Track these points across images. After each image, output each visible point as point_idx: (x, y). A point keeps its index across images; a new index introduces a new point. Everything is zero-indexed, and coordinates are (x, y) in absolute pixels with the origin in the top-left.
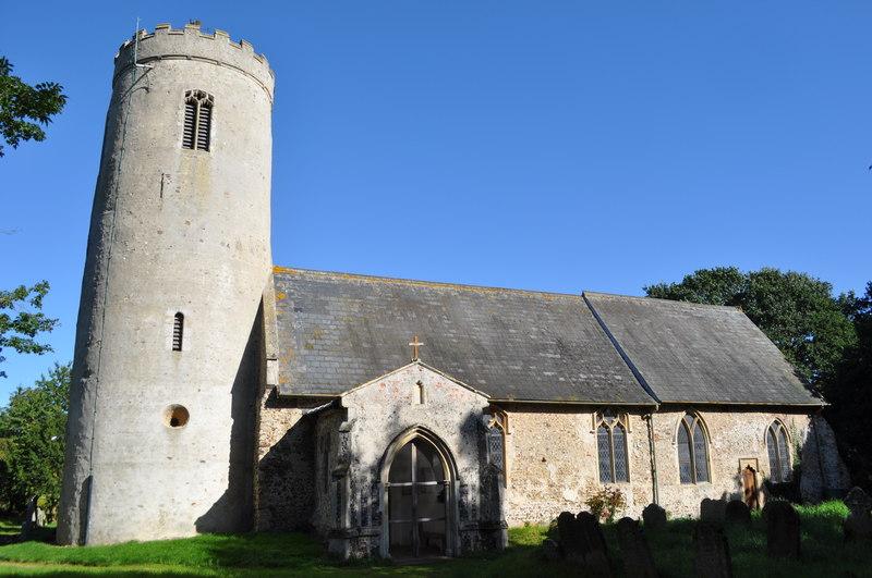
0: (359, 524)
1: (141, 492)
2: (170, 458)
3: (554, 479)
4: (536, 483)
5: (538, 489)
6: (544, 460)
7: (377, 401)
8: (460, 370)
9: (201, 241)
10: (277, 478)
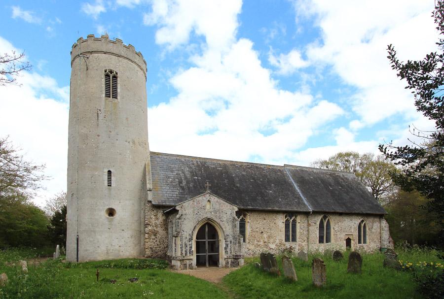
0: (184, 255)
3: (266, 240)
6: (262, 232)
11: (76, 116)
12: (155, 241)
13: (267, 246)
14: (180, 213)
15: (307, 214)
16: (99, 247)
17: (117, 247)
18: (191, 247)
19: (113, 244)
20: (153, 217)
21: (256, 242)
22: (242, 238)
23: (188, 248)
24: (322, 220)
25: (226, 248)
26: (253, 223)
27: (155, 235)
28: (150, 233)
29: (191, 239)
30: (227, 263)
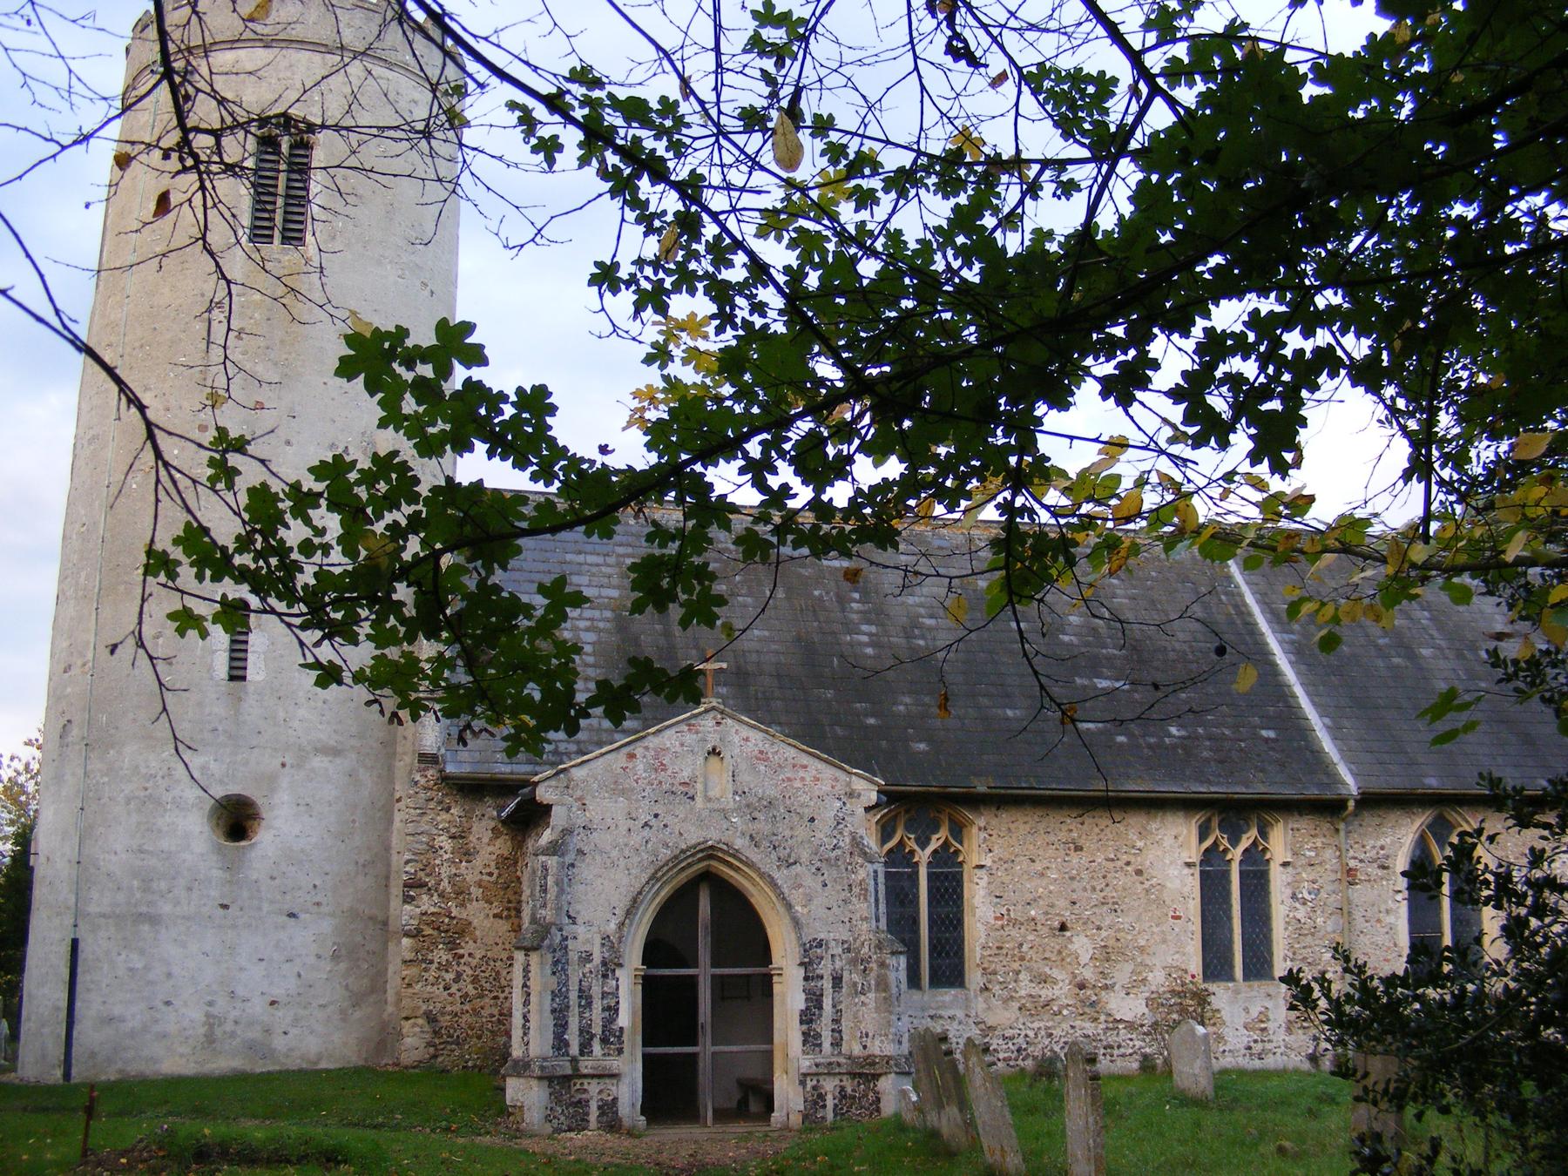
0: (574, 1049)
1: (169, 975)
2: (225, 907)
3: (1088, 974)
4: (1044, 980)
5: (1046, 993)
6: (1063, 928)
7: (617, 789)
8: (872, 721)
9: (288, 443)
10: (441, 955)
11: (113, 339)
12: (450, 976)
13: (1091, 1008)
14: (558, 817)
15: (1329, 808)
16: (168, 1003)
17: (258, 1007)
18: (613, 1010)
19: (240, 991)
20: (444, 842)
21: (1025, 987)
22: (903, 960)
23: (597, 1014)
24: (1421, 843)
25: (807, 1017)
26: (1008, 870)
27: (452, 945)
28: (428, 931)
29: (609, 968)
30: (817, 1100)
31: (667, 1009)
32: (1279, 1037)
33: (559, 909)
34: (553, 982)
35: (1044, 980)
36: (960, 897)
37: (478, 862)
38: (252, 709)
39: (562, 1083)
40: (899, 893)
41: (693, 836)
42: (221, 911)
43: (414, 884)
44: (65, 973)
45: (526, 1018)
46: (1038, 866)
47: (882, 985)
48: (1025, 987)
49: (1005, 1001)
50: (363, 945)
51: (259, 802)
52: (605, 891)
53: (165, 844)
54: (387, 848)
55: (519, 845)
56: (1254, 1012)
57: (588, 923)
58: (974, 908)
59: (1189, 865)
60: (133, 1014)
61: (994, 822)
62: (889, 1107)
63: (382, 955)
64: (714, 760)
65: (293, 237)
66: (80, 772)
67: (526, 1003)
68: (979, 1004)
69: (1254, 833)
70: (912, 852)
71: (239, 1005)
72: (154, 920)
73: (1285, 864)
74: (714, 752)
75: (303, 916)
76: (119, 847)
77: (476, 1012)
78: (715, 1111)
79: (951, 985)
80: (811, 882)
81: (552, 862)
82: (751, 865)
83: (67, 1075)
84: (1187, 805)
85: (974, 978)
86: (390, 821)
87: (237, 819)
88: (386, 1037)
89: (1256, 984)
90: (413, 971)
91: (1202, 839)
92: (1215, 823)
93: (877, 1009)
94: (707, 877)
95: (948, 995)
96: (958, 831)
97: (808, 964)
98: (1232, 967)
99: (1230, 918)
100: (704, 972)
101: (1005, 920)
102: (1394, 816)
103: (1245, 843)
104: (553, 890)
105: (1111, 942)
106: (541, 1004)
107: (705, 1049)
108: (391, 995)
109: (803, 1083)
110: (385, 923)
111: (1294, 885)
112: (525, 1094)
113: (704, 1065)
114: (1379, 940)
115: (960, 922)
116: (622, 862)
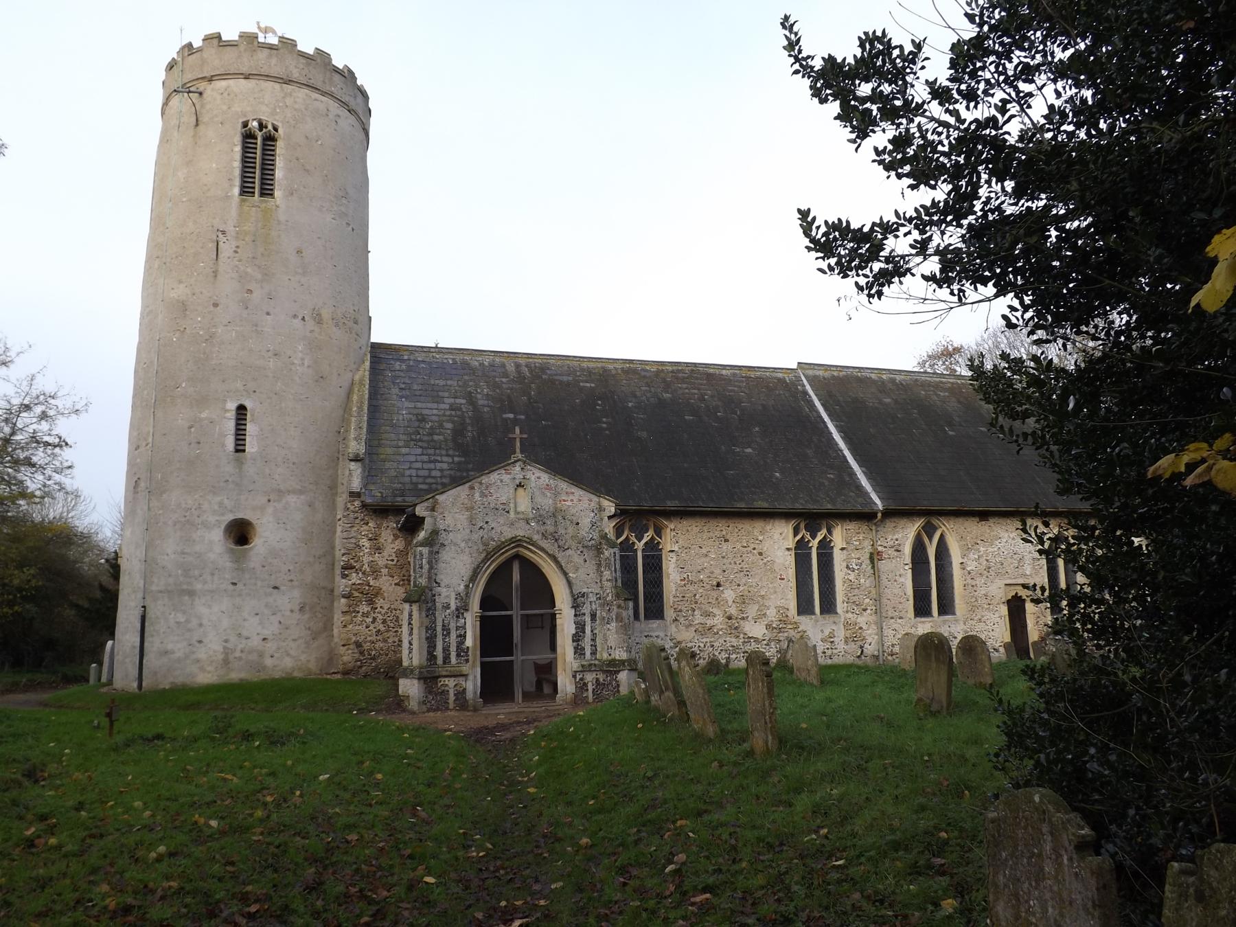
1: (201, 625)
2: (234, 584)
3: (733, 611)
4: (708, 614)
5: (710, 622)
6: (718, 585)
9: (268, 314)
10: (364, 608)
13: (735, 630)
15: (866, 517)
16: (200, 642)
20: (365, 543)
26: (687, 552)
27: (371, 602)
31: (495, 635)
32: (841, 646)
33: (429, 578)
34: (427, 622)
35: (708, 614)
36: (661, 568)
37: (385, 554)
38: (250, 469)
39: (429, 678)
40: (628, 566)
41: (509, 534)
42: (232, 587)
43: (348, 567)
44: (138, 626)
45: (411, 644)
46: (704, 551)
47: (619, 618)
48: (698, 618)
49: (688, 627)
50: (319, 603)
51: (254, 522)
52: (457, 571)
53: (197, 548)
54: (333, 548)
55: (408, 544)
56: (827, 633)
57: (448, 586)
58: (668, 575)
59: (788, 549)
60: (178, 647)
61: (679, 526)
62: (624, 690)
63: (330, 609)
64: (520, 490)
65: (267, 192)
66: (146, 508)
67: (411, 634)
68: (673, 629)
69: (824, 531)
70: (633, 543)
71: (244, 641)
72: (191, 593)
73: (842, 549)
74: (520, 485)
75: (283, 588)
76: (169, 551)
77: (385, 641)
78: (524, 693)
79: (657, 618)
80: (578, 559)
81: (425, 550)
82: (542, 550)
83: (140, 686)
84: (786, 515)
85: (669, 613)
86: (335, 532)
87: (240, 533)
88: (331, 657)
89: (827, 616)
90: (348, 618)
91: (795, 534)
92: (802, 525)
93: (617, 632)
94: (517, 556)
95: (655, 624)
96: (659, 532)
97: (576, 606)
98: (813, 607)
99: (812, 579)
100: (516, 613)
101: (687, 581)
102: (903, 522)
103: (820, 537)
104: (426, 567)
105: (746, 593)
106: (419, 634)
107: (518, 658)
108: (336, 631)
109: (574, 677)
110: (332, 591)
111: (848, 560)
112: (410, 688)
113: (517, 668)
114: (896, 591)
115: (661, 582)
116: (467, 550)
